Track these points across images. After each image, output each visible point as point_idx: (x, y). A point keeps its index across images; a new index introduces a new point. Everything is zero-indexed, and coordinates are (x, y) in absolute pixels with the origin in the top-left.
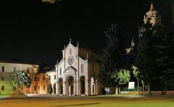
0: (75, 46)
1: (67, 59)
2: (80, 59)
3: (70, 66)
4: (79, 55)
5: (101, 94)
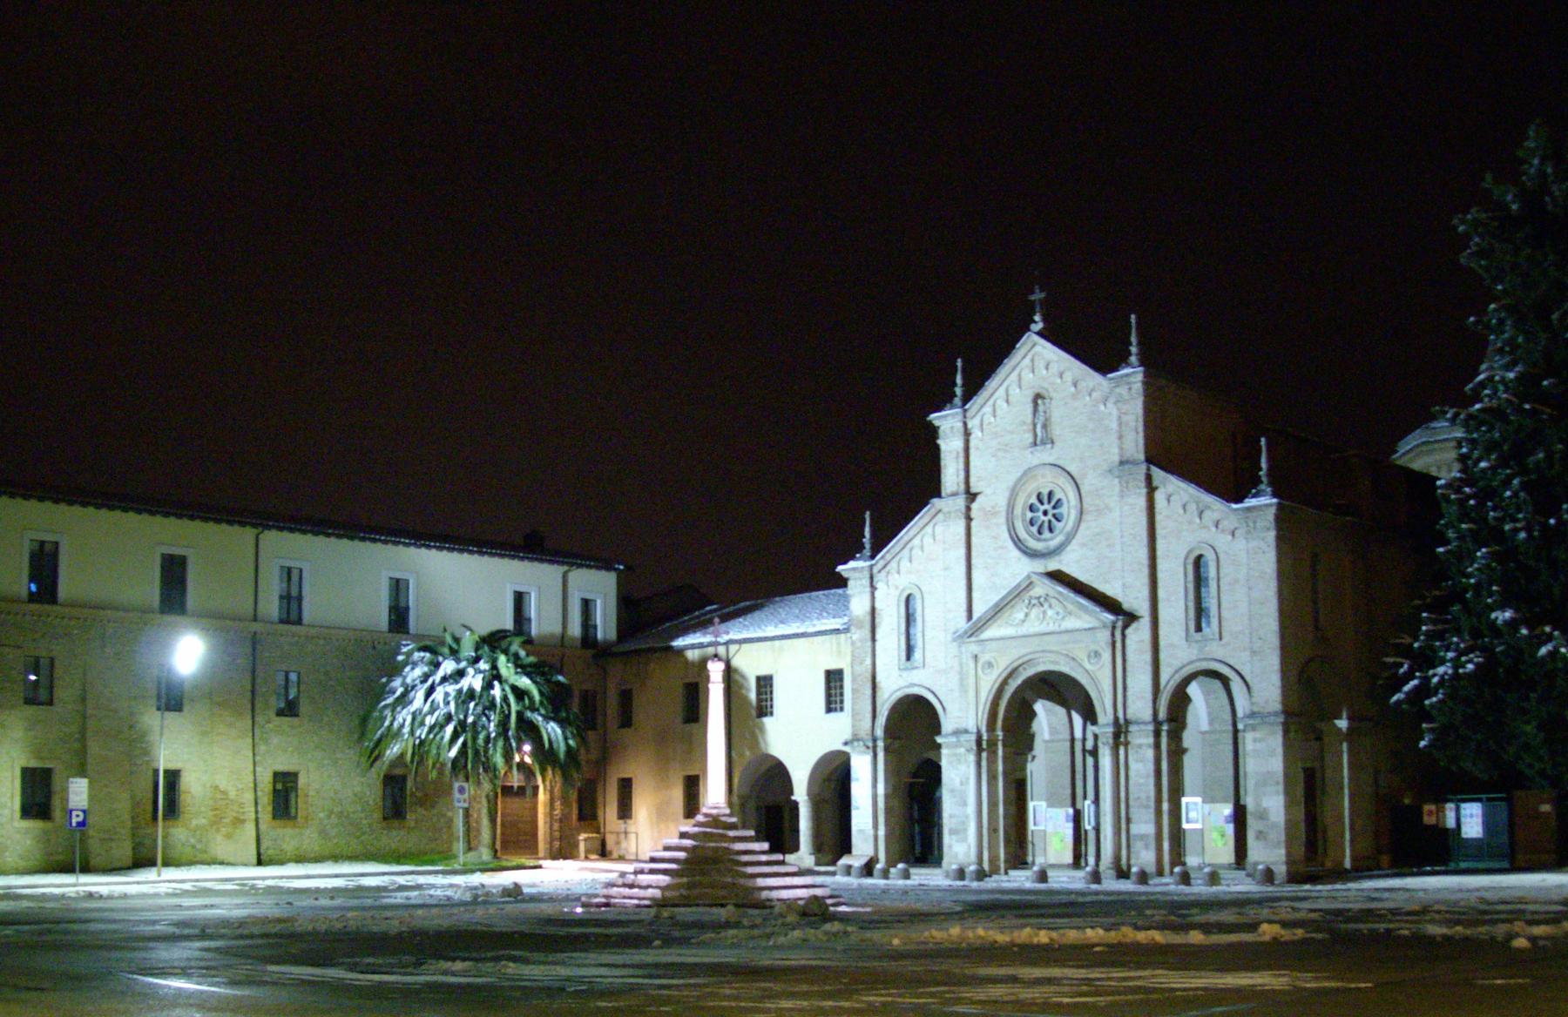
0: (1103, 359)
1: (993, 496)
2: (1176, 492)
3: (1041, 566)
4: (1150, 460)
5: (1385, 859)
